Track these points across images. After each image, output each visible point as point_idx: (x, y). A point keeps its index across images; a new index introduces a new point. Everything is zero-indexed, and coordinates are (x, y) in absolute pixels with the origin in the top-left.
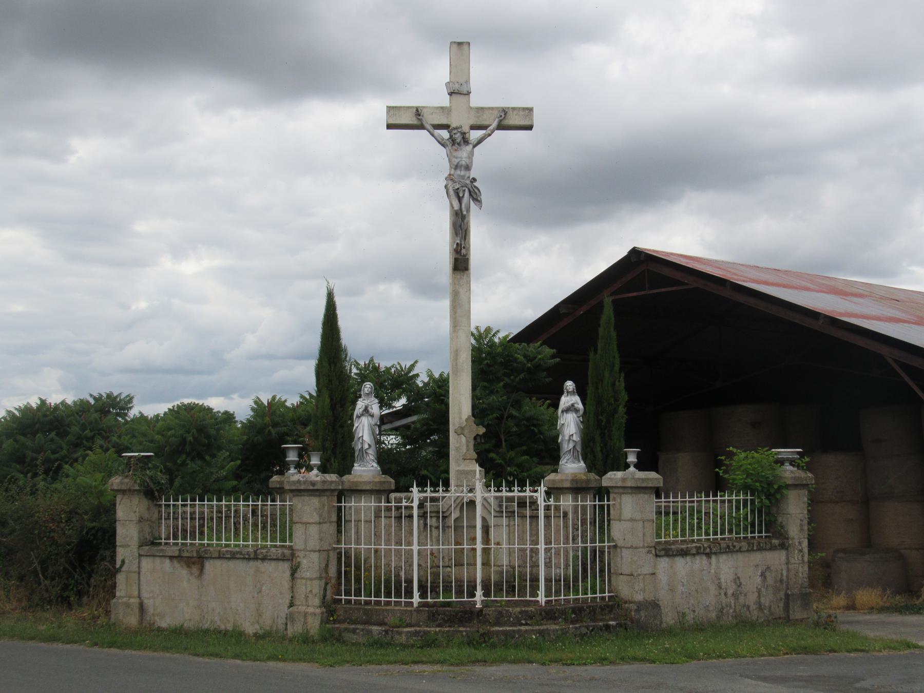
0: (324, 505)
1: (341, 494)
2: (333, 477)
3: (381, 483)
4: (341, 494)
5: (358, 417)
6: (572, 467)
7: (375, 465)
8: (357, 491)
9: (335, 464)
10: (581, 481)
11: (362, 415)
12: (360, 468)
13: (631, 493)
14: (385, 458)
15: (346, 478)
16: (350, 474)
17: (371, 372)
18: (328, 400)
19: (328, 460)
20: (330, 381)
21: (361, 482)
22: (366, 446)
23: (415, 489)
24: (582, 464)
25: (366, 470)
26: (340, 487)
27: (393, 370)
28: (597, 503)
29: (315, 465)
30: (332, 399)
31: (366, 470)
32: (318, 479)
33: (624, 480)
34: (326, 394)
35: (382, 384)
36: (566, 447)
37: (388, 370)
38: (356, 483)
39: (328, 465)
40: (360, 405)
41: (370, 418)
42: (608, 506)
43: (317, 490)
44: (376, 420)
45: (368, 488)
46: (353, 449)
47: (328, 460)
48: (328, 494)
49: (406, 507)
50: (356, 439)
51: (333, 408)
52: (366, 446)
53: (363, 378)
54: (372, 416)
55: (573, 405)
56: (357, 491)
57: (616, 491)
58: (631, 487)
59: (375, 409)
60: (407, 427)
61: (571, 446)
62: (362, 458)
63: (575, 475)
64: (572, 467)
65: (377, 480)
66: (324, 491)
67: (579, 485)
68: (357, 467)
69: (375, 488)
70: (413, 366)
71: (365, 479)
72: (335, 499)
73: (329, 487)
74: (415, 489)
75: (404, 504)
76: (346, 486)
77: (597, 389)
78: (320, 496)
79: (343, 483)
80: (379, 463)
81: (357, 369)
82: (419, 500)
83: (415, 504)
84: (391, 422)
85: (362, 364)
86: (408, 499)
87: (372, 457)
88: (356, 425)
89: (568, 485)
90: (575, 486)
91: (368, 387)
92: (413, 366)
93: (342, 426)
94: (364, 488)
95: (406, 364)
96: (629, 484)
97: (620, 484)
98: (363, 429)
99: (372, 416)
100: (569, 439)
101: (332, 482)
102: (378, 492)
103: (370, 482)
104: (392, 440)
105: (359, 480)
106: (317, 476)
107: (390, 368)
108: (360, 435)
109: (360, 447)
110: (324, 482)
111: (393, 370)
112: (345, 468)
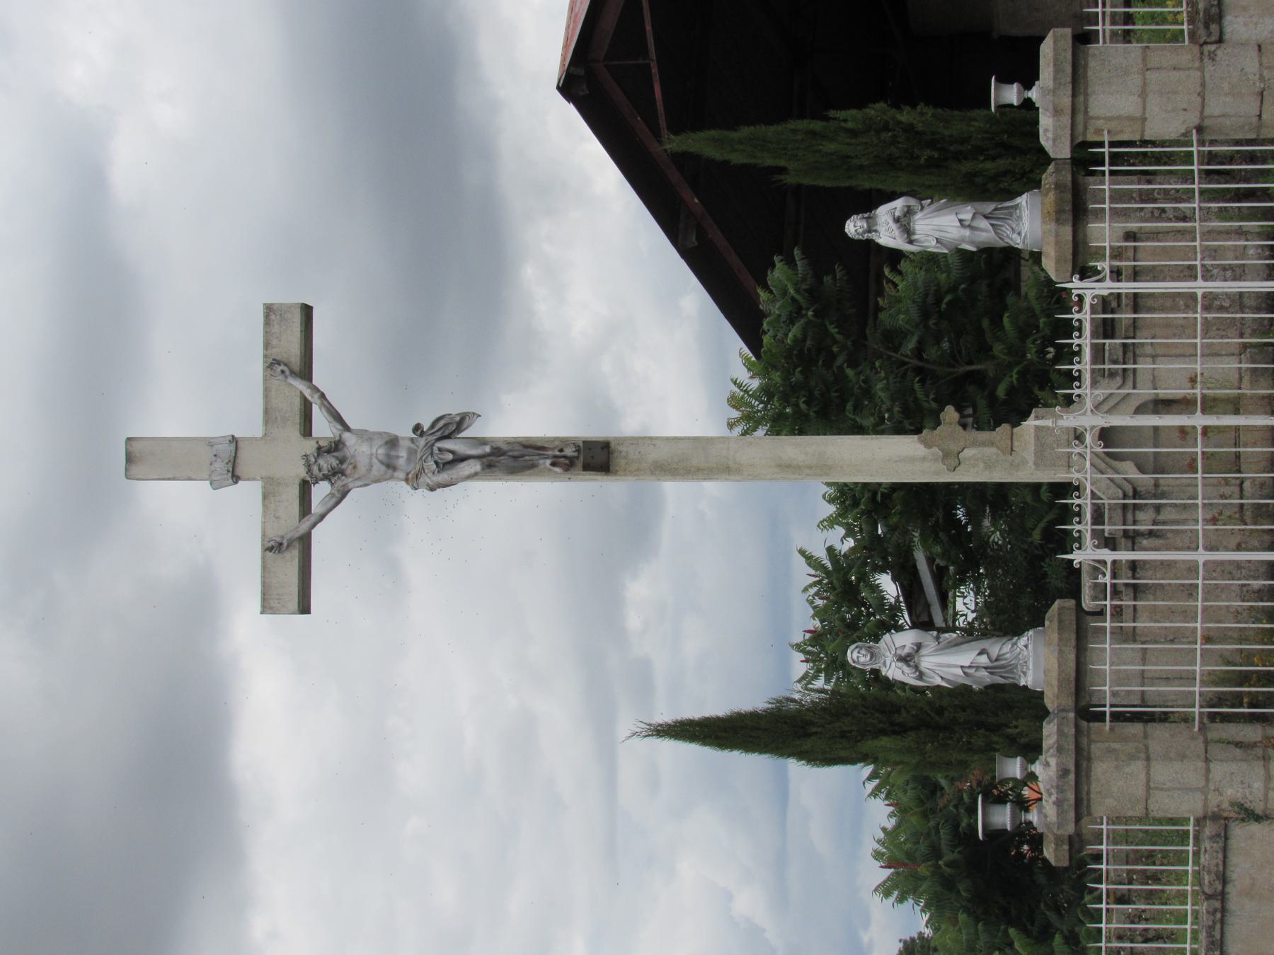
1: (1087, 713)
2: (1050, 731)
3: (1061, 629)
4: (1087, 713)
5: (921, 676)
6: (1029, 223)
7: (1023, 641)
8: (1080, 681)
9: (1021, 726)
10: (1059, 203)
11: (917, 667)
12: (1030, 673)
13: (1086, 95)
15: (1050, 703)
16: (1042, 693)
17: (823, 648)
18: (885, 741)
19: (1012, 740)
20: (843, 735)
22: (984, 660)
24: (1023, 200)
25: (1033, 659)
26: (1072, 715)
27: (819, 602)
28: (1107, 625)
29: (1024, 768)
30: (883, 732)
31: (1033, 659)
32: (1053, 762)
33: (1057, 112)
34: (870, 745)
36: (985, 234)
37: (819, 613)
38: (1062, 682)
39: (1023, 740)
40: (894, 671)
41: (923, 652)
45: (1072, 657)
47: (1012, 740)
48: (1084, 741)
49: (1114, 576)
50: (967, 682)
51: (899, 730)
52: (984, 660)
54: (919, 646)
55: (897, 220)
56: (1080, 681)
57: (1080, 128)
58: (1074, 95)
60: (939, 575)
61: (984, 224)
62: (1010, 668)
63: (1045, 216)
64: (1029, 223)
65: (1055, 636)
66: (1078, 749)
67: (1068, 207)
68: (1028, 679)
69: (1073, 642)
70: (810, 559)
73: (1072, 740)
75: (1107, 580)
76: (1069, 702)
77: (861, 167)
78: (1089, 759)
80: (1018, 632)
82: (1097, 547)
83: (1108, 555)
84: (927, 606)
87: (1007, 648)
89: (1067, 231)
90: (1069, 217)
91: (856, 656)
93: (940, 711)
96: (1066, 101)
97: (1066, 120)
98: (948, 664)
99: (919, 646)
100: (970, 227)
101: (1060, 733)
102: (1081, 633)
103: (1061, 652)
105: (1055, 674)
106: (1047, 764)
108: (959, 671)
109: (984, 673)
110: (1060, 750)
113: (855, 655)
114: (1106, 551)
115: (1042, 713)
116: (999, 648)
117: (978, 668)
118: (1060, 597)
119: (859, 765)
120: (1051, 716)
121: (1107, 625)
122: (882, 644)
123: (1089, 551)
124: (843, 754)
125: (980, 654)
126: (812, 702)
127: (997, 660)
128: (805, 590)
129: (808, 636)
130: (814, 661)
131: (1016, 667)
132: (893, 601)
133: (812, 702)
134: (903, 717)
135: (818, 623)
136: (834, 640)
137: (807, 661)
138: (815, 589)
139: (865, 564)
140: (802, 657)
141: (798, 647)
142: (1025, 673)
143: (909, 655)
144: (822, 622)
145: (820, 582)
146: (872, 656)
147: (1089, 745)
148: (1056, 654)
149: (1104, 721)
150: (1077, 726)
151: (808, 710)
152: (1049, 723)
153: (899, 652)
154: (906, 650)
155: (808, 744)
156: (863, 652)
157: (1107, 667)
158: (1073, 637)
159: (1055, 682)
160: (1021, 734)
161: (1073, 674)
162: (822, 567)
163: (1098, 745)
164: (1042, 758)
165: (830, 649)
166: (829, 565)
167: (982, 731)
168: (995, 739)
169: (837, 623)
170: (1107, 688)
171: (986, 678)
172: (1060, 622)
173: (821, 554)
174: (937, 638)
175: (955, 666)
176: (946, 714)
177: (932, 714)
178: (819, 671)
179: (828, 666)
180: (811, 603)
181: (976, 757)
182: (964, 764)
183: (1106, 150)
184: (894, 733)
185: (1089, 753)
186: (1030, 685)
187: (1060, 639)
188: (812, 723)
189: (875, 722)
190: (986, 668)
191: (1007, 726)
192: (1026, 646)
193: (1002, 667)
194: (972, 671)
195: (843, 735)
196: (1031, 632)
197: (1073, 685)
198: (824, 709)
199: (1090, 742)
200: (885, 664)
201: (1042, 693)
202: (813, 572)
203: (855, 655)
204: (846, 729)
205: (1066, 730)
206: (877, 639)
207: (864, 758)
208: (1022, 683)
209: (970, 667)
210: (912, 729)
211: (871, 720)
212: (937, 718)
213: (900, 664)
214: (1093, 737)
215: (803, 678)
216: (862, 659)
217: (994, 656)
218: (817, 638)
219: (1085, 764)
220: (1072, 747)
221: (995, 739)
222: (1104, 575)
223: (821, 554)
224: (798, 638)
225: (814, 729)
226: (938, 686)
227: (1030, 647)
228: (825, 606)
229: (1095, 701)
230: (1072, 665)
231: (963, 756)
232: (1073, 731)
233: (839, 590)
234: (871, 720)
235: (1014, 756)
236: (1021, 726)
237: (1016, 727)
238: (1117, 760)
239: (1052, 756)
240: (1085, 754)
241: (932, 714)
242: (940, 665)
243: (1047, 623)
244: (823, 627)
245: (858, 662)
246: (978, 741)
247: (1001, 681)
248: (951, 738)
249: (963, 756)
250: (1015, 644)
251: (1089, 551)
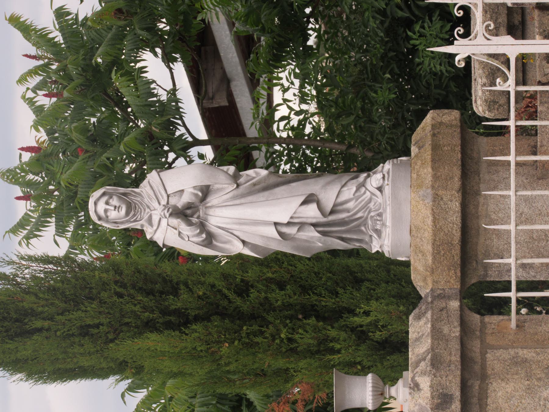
0: (517, 362)
1: (481, 297)
2: (419, 330)
3: (437, 160)
4: (481, 297)
5: (210, 239)
7: (375, 180)
8: (467, 243)
9: (375, 311)
11: (202, 226)
12: (387, 232)
14: (355, 142)
15: (422, 282)
16: (407, 264)
17: (52, 176)
18: (153, 341)
19: (361, 335)
20: (85, 331)
21: (437, 229)
22: (311, 212)
23: (461, 49)
25: (393, 210)
26: (455, 304)
27: (43, 101)
28: (511, 158)
29: (379, 393)
30: (150, 326)
31: (393, 210)
32: (425, 383)
34: (127, 347)
35: (93, 140)
37: (42, 117)
38: (439, 246)
39: (378, 335)
40: (168, 233)
41: (213, 200)
42: (522, 286)
43: (464, 387)
44: (222, 179)
45: (456, 206)
46: (317, 258)
47: (361, 335)
48: (475, 346)
49: (522, 80)
50: (286, 248)
51: (180, 322)
52: (311, 212)
53: (69, 208)
54: (206, 192)
56: (467, 243)
59: (181, 178)
60: (246, 45)
62: (354, 224)
65: (427, 172)
66: (466, 360)
68: (386, 242)
69: (457, 182)
70: (25, 29)
71: (425, 213)
72: (493, 320)
73: (455, 346)
74: (461, 49)
75: (510, 85)
76: (451, 282)
78: (484, 377)
79: (440, 296)
80: (368, 167)
81: (41, 224)
82: (496, 33)
83: (511, 47)
84: (226, 81)
85: (22, 208)
86: (493, 74)
87: (349, 192)
88: (237, 248)
91: (105, 208)
92: (25, 29)
93: (243, 289)
94: (455, 218)
95: (20, 54)
98: (257, 219)
99: (206, 192)
101: (436, 334)
102: (470, 179)
103: (436, 198)
104: (290, 100)
105: (428, 234)
106: (415, 387)
107: (38, 110)
108: (272, 232)
109: (312, 234)
110: (436, 363)
111: (43, 101)
112: (392, 278)
113: (101, 207)
114: (509, 39)
115: (410, 299)
116: (333, 191)
117: (302, 225)
118: (435, 107)
119: (112, 379)
120: (422, 306)
121: (511, 158)
122: (144, 188)
123: (480, 40)
124: (85, 362)
125: (304, 203)
126: (34, 278)
127: (332, 212)
128: (22, 80)
129: (27, 156)
130: (37, 198)
131: (365, 224)
132: (164, 97)
133: (34, 278)
134: (183, 301)
135: (43, 136)
136: (71, 163)
137: (26, 197)
138: (38, 79)
139: (120, 37)
140: (18, 191)
141: (12, 176)
142: (378, 233)
143: (189, 206)
144: (49, 133)
145: (45, 68)
146: (130, 207)
147: (483, 354)
148: (429, 201)
149: (509, 313)
150: (463, 324)
151: (27, 292)
152: (418, 318)
153: (173, 201)
154: (186, 199)
155: (27, 348)
156: (115, 201)
157: (512, 227)
158: (457, 172)
159: (428, 248)
160: (375, 324)
161: (457, 235)
162: (51, 44)
163: (499, 353)
164: (408, 375)
165: (64, 178)
166: (60, 39)
167: (312, 321)
168: (333, 333)
169: (75, 136)
170: (511, 261)
171: (313, 241)
172: (435, 148)
173: (46, 21)
174: (235, 178)
175: (265, 223)
176: (253, 294)
177: (232, 296)
178: (47, 213)
179: (60, 205)
180: (31, 102)
181: (302, 364)
182: (285, 375)
183: (513, 295)
184: (169, 326)
185: (484, 367)
186: (387, 251)
187: (436, 177)
188: (33, 313)
189: (137, 308)
190: (314, 225)
191: (351, 312)
192: (380, 189)
193: (342, 223)
194: (292, 231)
195: (85, 331)
196: (388, 166)
197: (457, 251)
198: (52, 290)
199: (485, 347)
200: (150, 221)
201: (407, 264)
202: (33, 51)
203: (101, 207)
204: (89, 322)
205: (446, 330)
206: (137, 181)
207: (119, 368)
208: (375, 248)
209: (289, 224)
210: (197, 319)
211: (129, 307)
212: (238, 301)
213: (175, 221)
214: (490, 340)
215: (21, 225)
216: (113, 214)
217: (328, 205)
218: (41, 158)
219: (476, 385)
220: (456, 358)
221: (333, 333)
222: (506, 79)
223: (46, 21)
224: (15, 159)
225: (39, 324)
226: (240, 256)
227: (387, 190)
228: (54, 107)
229: (493, 277)
230: (454, 218)
231: (281, 363)
232: (456, 332)
233: (78, 81)
234: (129, 307)
235: (364, 371)
236: (375, 311)
237: (367, 313)
238: (529, 377)
239: (423, 373)
240: (477, 368)
241: (232, 296)
242: (242, 222)
243: (414, 150)
244: (52, 139)
245: (107, 220)
246: (305, 339)
247: (340, 245)
248: (262, 333)
249: (281, 363)
250: (363, 185)
251: (480, 40)
